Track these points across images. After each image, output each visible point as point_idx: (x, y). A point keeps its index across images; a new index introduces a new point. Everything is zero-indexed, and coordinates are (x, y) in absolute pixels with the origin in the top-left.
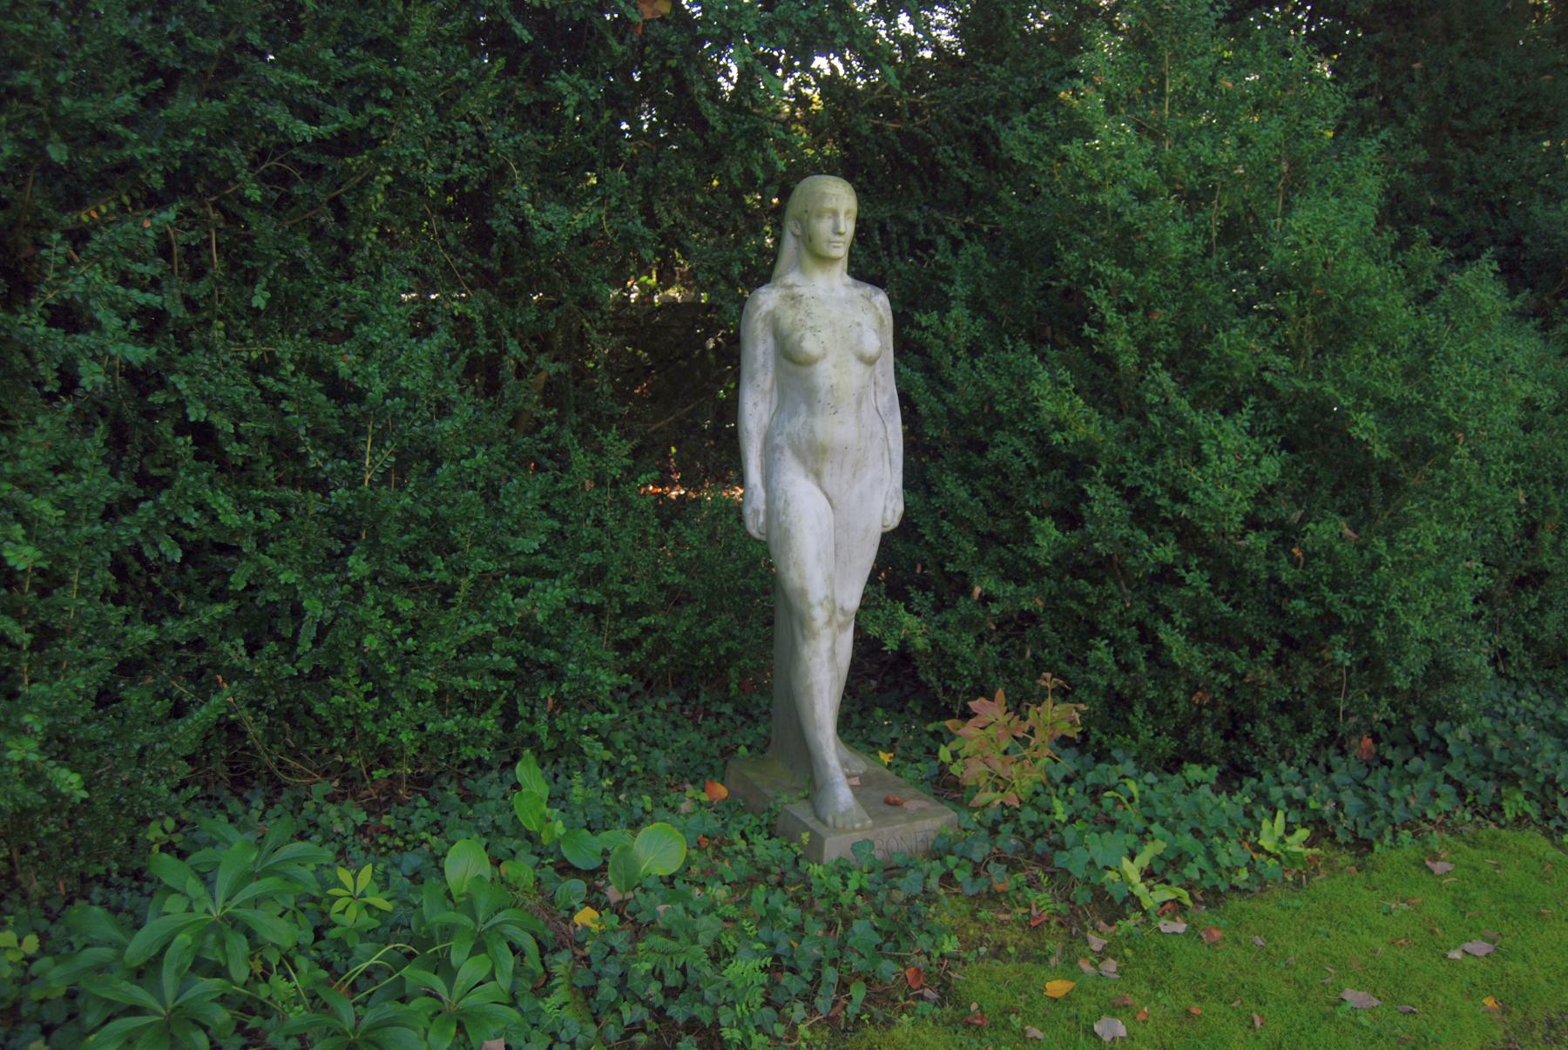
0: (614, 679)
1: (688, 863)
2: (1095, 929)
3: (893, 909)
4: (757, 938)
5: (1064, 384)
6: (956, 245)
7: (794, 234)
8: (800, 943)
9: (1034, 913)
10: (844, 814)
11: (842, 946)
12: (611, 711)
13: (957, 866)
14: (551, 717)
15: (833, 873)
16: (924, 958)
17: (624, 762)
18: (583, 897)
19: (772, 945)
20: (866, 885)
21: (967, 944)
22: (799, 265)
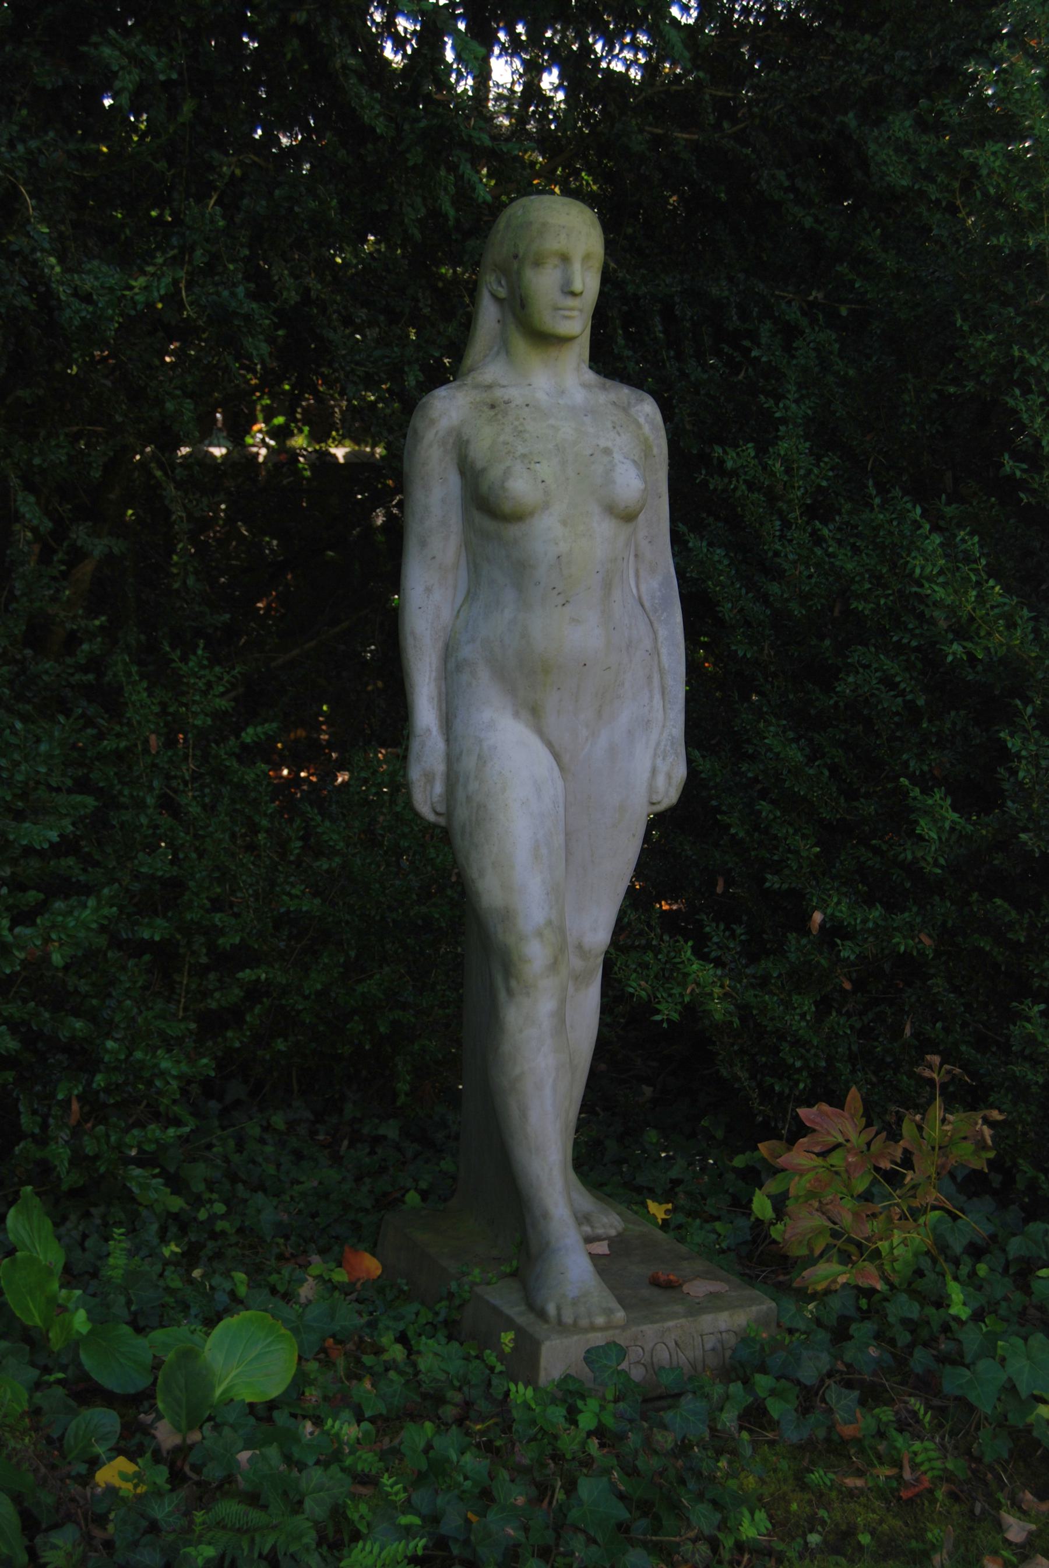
0: (184, 1067)
1: (300, 1381)
2: (1017, 1506)
3: (655, 1463)
4: (408, 1507)
5: (968, 558)
6: (789, 333)
7: (495, 297)
8: (482, 1514)
9: (907, 1475)
10: (575, 1302)
11: (560, 1526)
12: (178, 1122)
13: (773, 1392)
14: (76, 1132)
15: (554, 1401)
16: (704, 1548)
17: (202, 1215)
18: (112, 1443)
19: (433, 1519)
20: (609, 1421)
21: (782, 1526)
22: (505, 347)
